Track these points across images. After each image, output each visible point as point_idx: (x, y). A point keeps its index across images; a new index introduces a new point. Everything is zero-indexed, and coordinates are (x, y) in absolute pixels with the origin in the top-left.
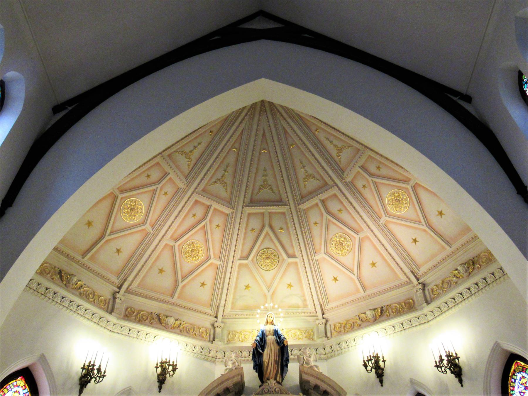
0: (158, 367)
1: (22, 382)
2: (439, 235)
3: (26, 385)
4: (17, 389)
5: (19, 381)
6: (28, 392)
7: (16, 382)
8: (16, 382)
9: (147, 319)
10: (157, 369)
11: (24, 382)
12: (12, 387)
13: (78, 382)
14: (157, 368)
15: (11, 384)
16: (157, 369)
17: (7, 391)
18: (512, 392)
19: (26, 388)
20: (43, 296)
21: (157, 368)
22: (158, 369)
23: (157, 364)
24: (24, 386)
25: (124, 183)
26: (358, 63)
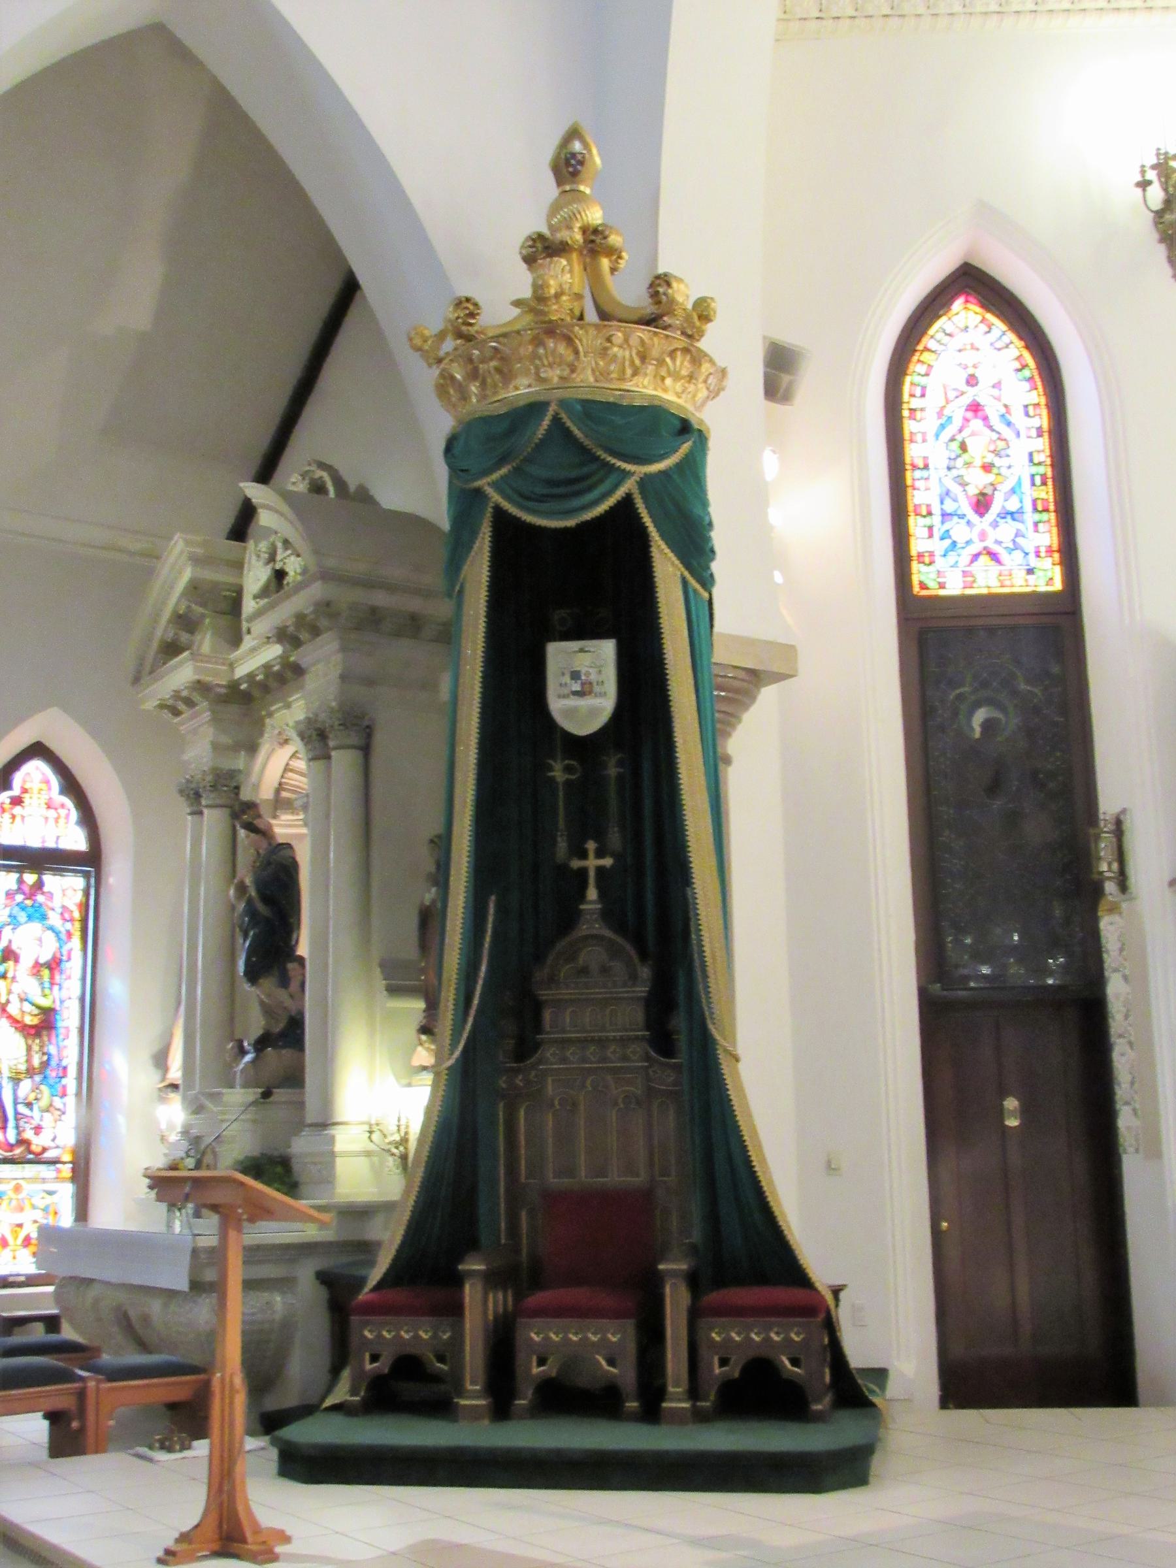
0: (1149, 183)
1: (971, 314)
2: (227, 1431)
3: (989, 316)
4: (961, 339)
5: (957, 314)
6: (1004, 333)
7: (949, 319)
8: (949, 319)
9: (707, 377)
10: (1144, 190)
11: (978, 309)
12: (946, 339)
13: (1155, 236)
14: (1144, 184)
15: (937, 331)
16: (1144, 190)
17: (933, 356)
18: (915, 403)
19: (990, 326)
20: (894, 23)
21: (1144, 184)
22: (1149, 189)
23: (1143, 172)
24: (983, 320)
25: (630, 325)
26: (667, 1493)
